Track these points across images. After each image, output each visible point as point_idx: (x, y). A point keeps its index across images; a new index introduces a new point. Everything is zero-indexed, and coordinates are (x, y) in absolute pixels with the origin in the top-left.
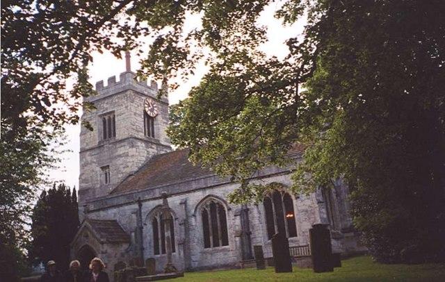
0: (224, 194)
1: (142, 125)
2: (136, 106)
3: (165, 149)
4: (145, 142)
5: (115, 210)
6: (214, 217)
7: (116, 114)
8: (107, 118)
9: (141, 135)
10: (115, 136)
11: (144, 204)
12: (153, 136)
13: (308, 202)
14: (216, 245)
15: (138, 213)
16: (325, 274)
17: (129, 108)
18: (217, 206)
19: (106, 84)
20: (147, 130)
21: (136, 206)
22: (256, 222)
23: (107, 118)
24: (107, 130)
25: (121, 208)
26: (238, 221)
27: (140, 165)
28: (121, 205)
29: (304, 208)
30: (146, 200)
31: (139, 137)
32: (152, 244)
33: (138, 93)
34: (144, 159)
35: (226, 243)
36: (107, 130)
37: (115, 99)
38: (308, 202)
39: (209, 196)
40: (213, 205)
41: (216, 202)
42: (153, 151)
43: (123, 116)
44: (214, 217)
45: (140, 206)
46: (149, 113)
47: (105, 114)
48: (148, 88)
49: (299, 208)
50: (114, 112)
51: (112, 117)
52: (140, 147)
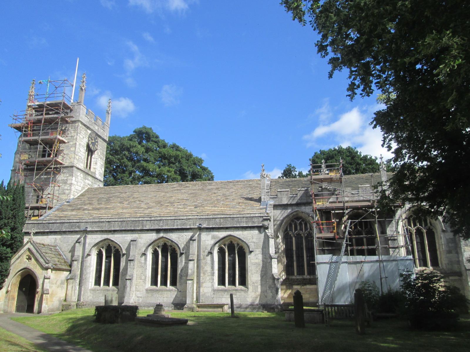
2: (82, 137)
3: (98, 183)
9: (82, 166)
12: (90, 168)
31: (80, 167)
33: (85, 125)
39: (162, 237)
46: (91, 146)
49: (253, 261)
52: (79, 178)
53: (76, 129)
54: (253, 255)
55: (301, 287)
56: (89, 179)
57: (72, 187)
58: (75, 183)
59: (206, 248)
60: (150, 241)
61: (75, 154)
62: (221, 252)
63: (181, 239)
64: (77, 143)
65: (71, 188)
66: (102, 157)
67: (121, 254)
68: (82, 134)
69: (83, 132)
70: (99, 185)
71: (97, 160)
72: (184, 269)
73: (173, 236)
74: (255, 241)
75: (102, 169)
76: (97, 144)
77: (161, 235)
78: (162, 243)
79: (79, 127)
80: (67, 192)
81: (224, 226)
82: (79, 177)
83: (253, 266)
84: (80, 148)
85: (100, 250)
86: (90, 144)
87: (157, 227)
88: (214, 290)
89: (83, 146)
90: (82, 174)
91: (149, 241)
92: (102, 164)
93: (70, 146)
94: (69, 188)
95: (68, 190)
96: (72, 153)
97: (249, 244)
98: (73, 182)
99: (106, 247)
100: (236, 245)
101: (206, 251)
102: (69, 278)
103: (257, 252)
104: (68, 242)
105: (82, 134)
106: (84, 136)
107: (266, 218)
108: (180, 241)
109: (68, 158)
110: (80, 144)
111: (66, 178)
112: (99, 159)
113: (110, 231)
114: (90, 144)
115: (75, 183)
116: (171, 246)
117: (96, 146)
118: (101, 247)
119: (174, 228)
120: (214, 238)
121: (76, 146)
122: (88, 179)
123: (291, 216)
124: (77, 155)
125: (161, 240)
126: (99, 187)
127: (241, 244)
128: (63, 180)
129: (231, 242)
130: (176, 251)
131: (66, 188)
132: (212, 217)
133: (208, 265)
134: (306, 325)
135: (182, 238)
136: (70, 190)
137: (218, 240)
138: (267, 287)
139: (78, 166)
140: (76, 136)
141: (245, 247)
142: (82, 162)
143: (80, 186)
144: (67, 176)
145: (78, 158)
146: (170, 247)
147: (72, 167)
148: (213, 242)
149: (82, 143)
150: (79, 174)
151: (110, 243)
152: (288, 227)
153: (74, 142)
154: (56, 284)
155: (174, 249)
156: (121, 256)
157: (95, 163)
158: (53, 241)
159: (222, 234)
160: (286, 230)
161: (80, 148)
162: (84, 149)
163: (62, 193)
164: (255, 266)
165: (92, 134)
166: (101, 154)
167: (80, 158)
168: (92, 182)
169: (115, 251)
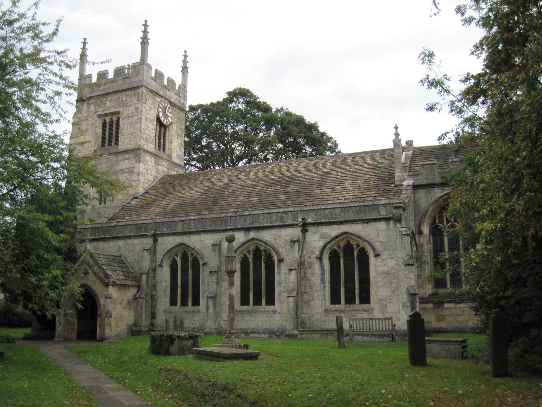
0: (275, 239)
1: (153, 135)
2: (149, 108)
3: (176, 169)
4: (155, 156)
5: (120, 243)
6: (257, 268)
7: (122, 116)
8: (108, 120)
9: (151, 147)
10: (365, 299)
11: (161, 239)
12: (164, 149)
13: (391, 263)
14: (257, 302)
15: (153, 251)
16: (77, 329)
17: (139, 110)
18: (263, 253)
19: (111, 76)
20: (157, 141)
21: (296, 232)
22: (316, 280)
23: (108, 120)
24: (107, 136)
25: (129, 241)
26: (293, 276)
27: (147, 186)
28: (129, 237)
29: (385, 269)
30: (163, 235)
31: (149, 149)
32: (168, 292)
33: (152, 91)
34: (152, 178)
35: (271, 301)
36: (107, 136)
37: (123, 97)
38: (391, 263)
39: (253, 239)
40: (257, 252)
41: (262, 248)
42: (163, 169)
43: (130, 119)
44: (257, 268)
45: (155, 241)
46: (162, 119)
47: (106, 115)
48: (165, 87)
49: (379, 269)
50: (118, 113)
51: (115, 119)
52: (149, 163)
53: (139, 97)
54: (379, 260)
55: (456, 305)
56: (164, 163)
57: (141, 177)
58: (145, 171)
59: (313, 252)
61: (141, 132)
62: (334, 257)
63: (278, 241)
64: (143, 117)
65: (139, 178)
66: (180, 133)
67: (201, 264)
68: (148, 104)
69: (150, 101)
70: (178, 172)
72: (284, 283)
73: (267, 236)
74: (382, 241)
75: (180, 149)
78: (253, 247)
79: (144, 95)
80: (134, 184)
81: (337, 220)
82: (148, 162)
83: (380, 276)
85: (174, 259)
86: (160, 117)
88: (326, 310)
89: (151, 121)
90: (152, 159)
92: (180, 142)
93: (134, 122)
94: (136, 179)
95: (135, 181)
96: (138, 131)
97: (374, 244)
98: (141, 170)
99: (181, 255)
100: (355, 247)
101: (313, 256)
102: (137, 297)
103: (386, 257)
104: (134, 250)
105: (148, 104)
106: (152, 107)
107: (397, 205)
108: (277, 243)
109: (133, 138)
110: (147, 119)
111: (132, 166)
112: (176, 136)
113: (185, 233)
114: (162, 117)
115: (145, 171)
116: (265, 251)
117: (169, 119)
118: (175, 255)
119: (268, 225)
120: (324, 238)
121: (141, 120)
122: (162, 165)
123: (440, 202)
124: (143, 133)
126: (177, 173)
127: (363, 244)
128: (129, 168)
129: (348, 242)
130: (272, 257)
131: (133, 178)
133: (316, 276)
134: (429, 361)
136: (139, 180)
137: (328, 240)
138: (400, 306)
139: (146, 147)
140: (141, 108)
141: (199, 257)
142: (151, 143)
143: (152, 175)
144: (133, 162)
145: (145, 138)
146: (264, 253)
147: (139, 149)
148: (321, 243)
149: (150, 117)
150: (148, 158)
151: (186, 250)
152: (437, 218)
153: (139, 116)
154: (121, 304)
155: (270, 254)
156: (276, 264)
157: (170, 142)
158: (116, 249)
159: (334, 231)
160: (434, 222)
162: (153, 125)
164: (383, 275)
166: (177, 129)
167: (148, 136)
168: (168, 168)
169: (192, 260)
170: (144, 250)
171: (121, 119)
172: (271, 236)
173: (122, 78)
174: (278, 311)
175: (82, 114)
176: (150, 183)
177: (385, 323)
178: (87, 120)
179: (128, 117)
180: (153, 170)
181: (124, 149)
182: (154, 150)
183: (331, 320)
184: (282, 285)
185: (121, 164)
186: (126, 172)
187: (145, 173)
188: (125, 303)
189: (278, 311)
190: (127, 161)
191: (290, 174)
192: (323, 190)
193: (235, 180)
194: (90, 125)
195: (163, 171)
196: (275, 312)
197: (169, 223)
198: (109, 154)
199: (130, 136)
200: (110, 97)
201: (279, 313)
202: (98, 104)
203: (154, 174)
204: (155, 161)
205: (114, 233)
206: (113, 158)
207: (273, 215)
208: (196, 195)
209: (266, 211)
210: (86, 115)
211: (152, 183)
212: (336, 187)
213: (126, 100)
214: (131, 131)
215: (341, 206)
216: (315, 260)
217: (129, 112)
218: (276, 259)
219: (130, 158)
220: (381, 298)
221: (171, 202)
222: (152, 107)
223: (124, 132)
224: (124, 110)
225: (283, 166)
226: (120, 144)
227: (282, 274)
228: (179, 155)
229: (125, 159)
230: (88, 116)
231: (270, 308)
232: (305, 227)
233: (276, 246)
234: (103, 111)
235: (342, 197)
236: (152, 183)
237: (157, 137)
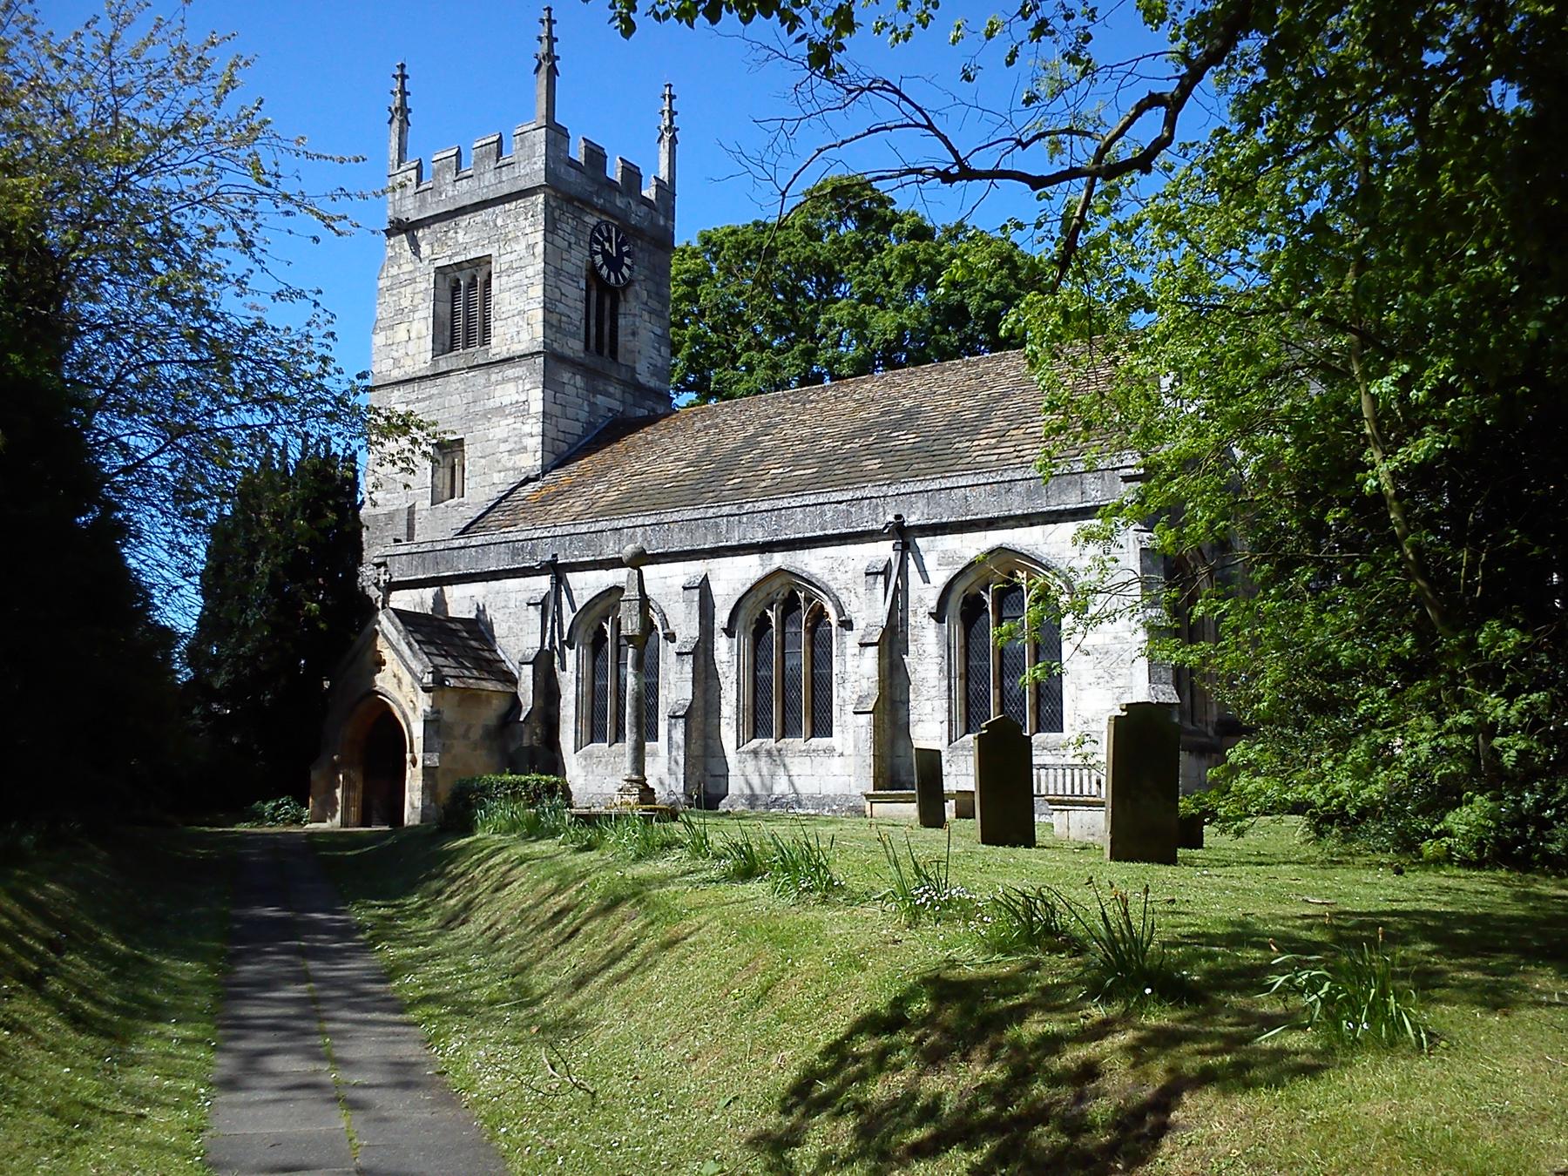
1: (577, 316)
7: (495, 267)
21: (884, 551)
35: (822, 727)
50: (486, 260)
56: (611, 389)
60: (744, 585)
63: (838, 574)
68: (561, 233)
71: (637, 319)
73: (811, 562)
75: (659, 351)
76: (627, 261)
77: (779, 560)
84: (560, 283)
87: (760, 537)
89: (572, 277)
90: (578, 377)
91: (739, 586)
93: (526, 281)
101: (922, 610)
105: (561, 233)
106: (573, 240)
109: (525, 326)
112: (646, 316)
114: (601, 267)
117: (625, 270)
125: (777, 583)
132: (938, 487)
133: (927, 660)
135: (841, 568)
142: (574, 335)
143: (578, 420)
144: (527, 387)
149: (568, 267)
154: (465, 736)
161: (560, 283)
162: (578, 287)
163: (518, 446)
165: (603, 228)
166: (649, 296)
168: (623, 402)
170: (529, 604)
171: (494, 276)
172: (824, 563)
173: (492, 167)
174: (839, 750)
175: (400, 266)
176: (570, 439)
177: (1073, 775)
178: (413, 281)
179: (511, 269)
180: (581, 407)
181: (505, 355)
182: (582, 355)
183: (964, 772)
184: (848, 685)
185: (497, 394)
186: (510, 414)
187: (559, 414)
188: (476, 733)
189: (839, 750)
190: (511, 386)
191: (907, 404)
192: (976, 443)
193: (775, 426)
194: (421, 295)
195: (610, 410)
196: (829, 751)
197: (586, 537)
198: (469, 368)
199: (517, 319)
200: (464, 220)
201: (842, 755)
202: (438, 240)
203: (583, 416)
204: (586, 384)
205: (461, 567)
206: (479, 377)
207: (826, 507)
208: (672, 468)
209: (812, 499)
210: (410, 267)
211: (579, 441)
212: (1012, 432)
213: (505, 226)
214: (521, 306)
215: (991, 480)
216: (925, 621)
217: (513, 257)
218: (833, 618)
219: (519, 378)
220: (1088, 715)
221: (611, 485)
222: (573, 240)
223: (503, 309)
224: (502, 252)
225: (899, 385)
226: (494, 341)
227: (848, 658)
228: (655, 366)
229: (505, 381)
230: (415, 270)
231: (819, 742)
232: (903, 535)
233: (834, 586)
234: (451, 257)
235: (1017, 457)
236: (579, 441)
237: (593, 322)
